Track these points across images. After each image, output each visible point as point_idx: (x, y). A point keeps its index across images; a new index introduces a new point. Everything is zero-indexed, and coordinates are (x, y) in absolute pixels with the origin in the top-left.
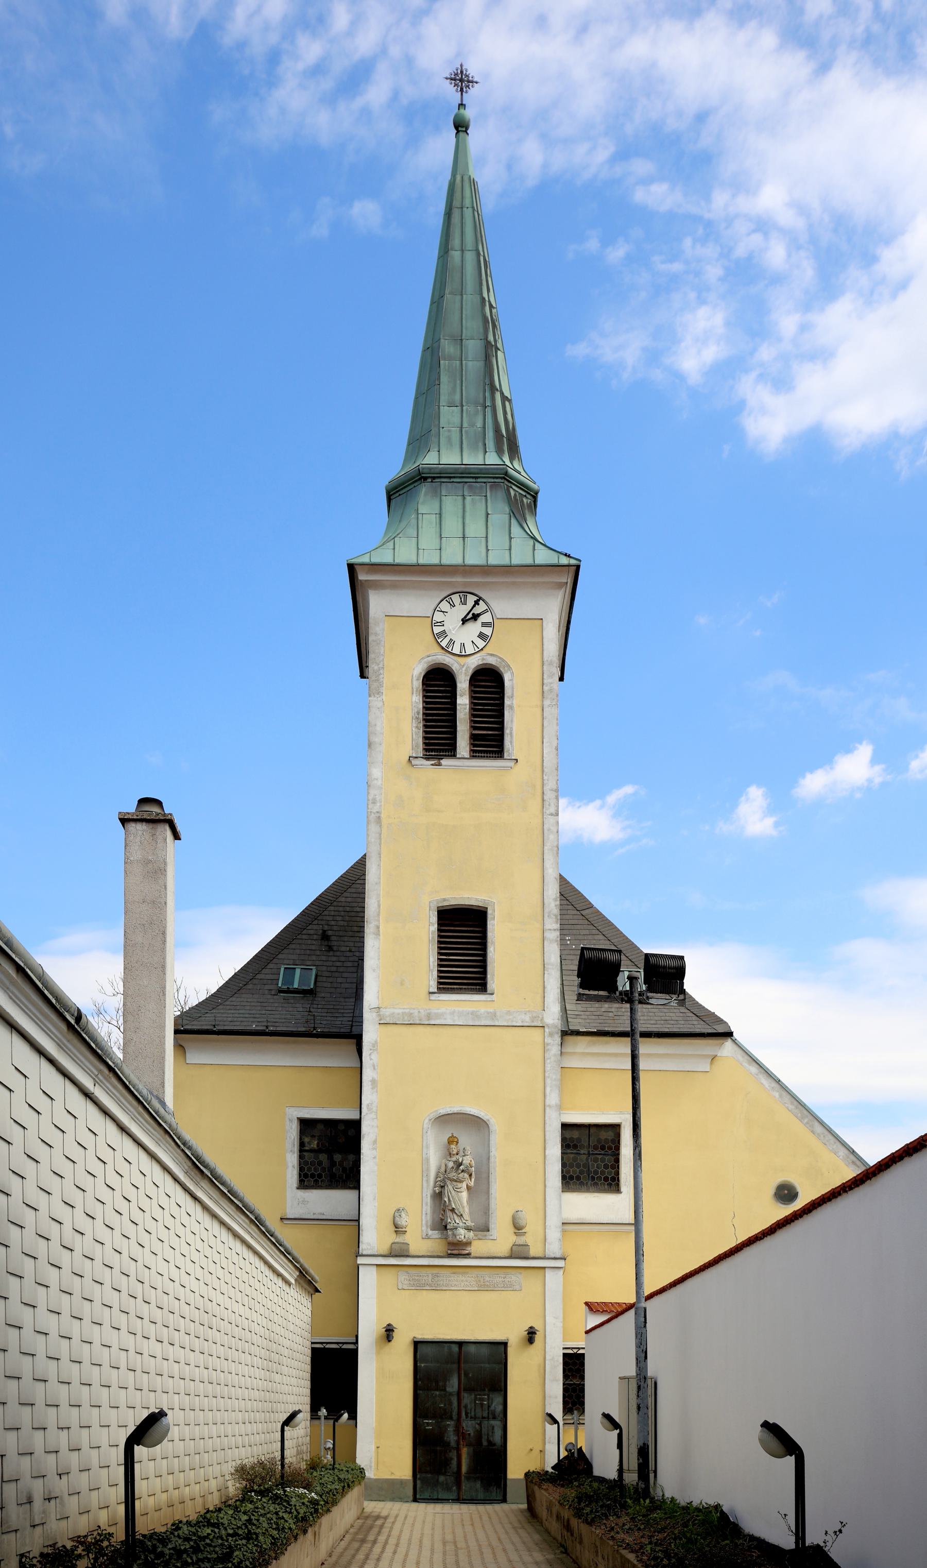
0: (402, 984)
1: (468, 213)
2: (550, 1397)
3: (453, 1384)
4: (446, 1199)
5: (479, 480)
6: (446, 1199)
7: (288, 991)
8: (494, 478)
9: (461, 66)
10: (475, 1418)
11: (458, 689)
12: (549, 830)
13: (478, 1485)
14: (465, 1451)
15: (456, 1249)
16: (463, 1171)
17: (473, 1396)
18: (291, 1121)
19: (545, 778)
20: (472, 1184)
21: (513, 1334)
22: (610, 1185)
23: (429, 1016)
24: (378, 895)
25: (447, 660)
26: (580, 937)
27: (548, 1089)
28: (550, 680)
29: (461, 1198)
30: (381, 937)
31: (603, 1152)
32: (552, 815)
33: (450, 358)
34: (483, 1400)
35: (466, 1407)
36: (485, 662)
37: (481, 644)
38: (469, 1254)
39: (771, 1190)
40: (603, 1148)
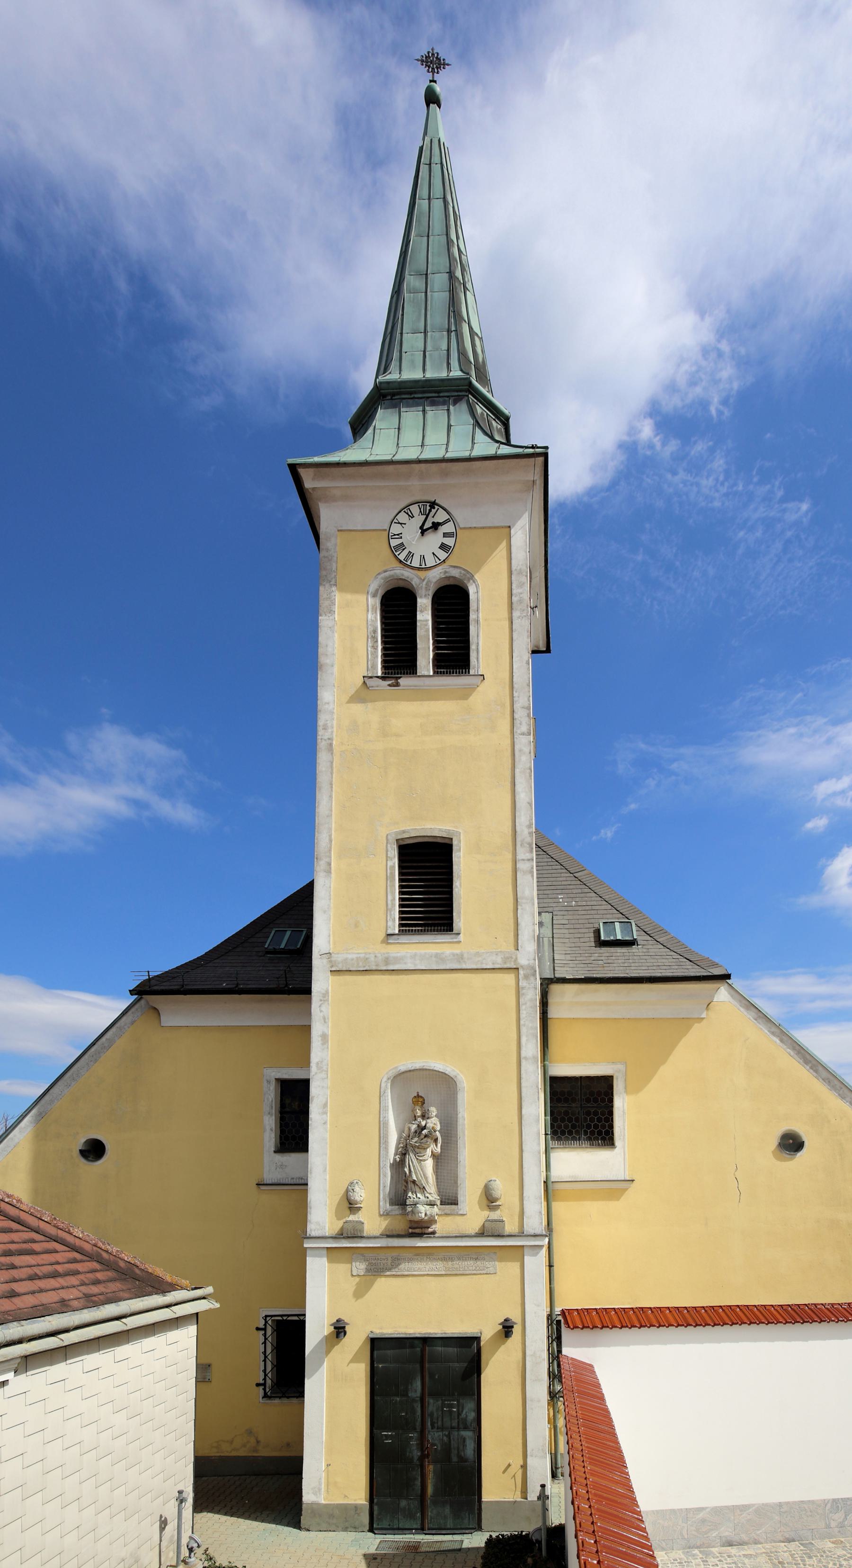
0: (356, 925)
1: (436, 169)
2: (532, 1400)
3: (416, 1388)
4: (407, 1170)
5: (441, 394)
6: (407, 1170)
7: (275, 952)
8: (457, 391)
9: (433, 49)
10: (442, 1428)
11: (418, 605)
12: (520, 750)
13: (447, 1510)
14: (430, 1469)
15: (419, 1229)
16: (426, 1136)
17: (440, 1403)
18: (269, 1082)
19: (515, 694)
20: (439, 1150)
21: (486, 1329)
22: (603, 1139)
23: (387, 961)
24: (330, 829)
25: (407, 574)
26: (572, 896)
27: (524, 1040)
28: (520, 591)
29: (425, 1168)
30: (333, 875)
31: (595, 1105)
32: (523, 734)
33: (415, 291)
34: (451, 1406)
35: (431, 1415)
36: (449, 578)
37: (442, 555)
38: (434, 1233)
39: (774, 1142)
40: (596, 1101)
